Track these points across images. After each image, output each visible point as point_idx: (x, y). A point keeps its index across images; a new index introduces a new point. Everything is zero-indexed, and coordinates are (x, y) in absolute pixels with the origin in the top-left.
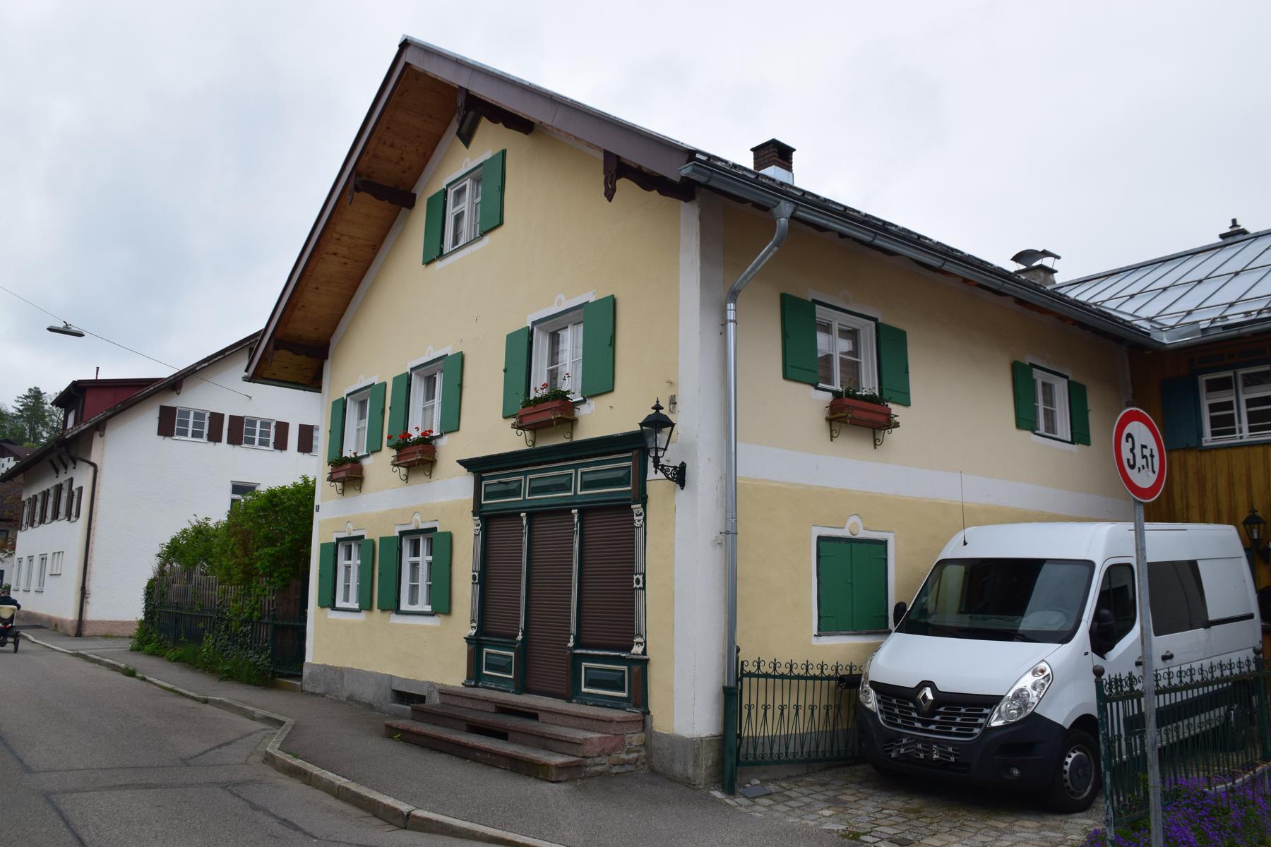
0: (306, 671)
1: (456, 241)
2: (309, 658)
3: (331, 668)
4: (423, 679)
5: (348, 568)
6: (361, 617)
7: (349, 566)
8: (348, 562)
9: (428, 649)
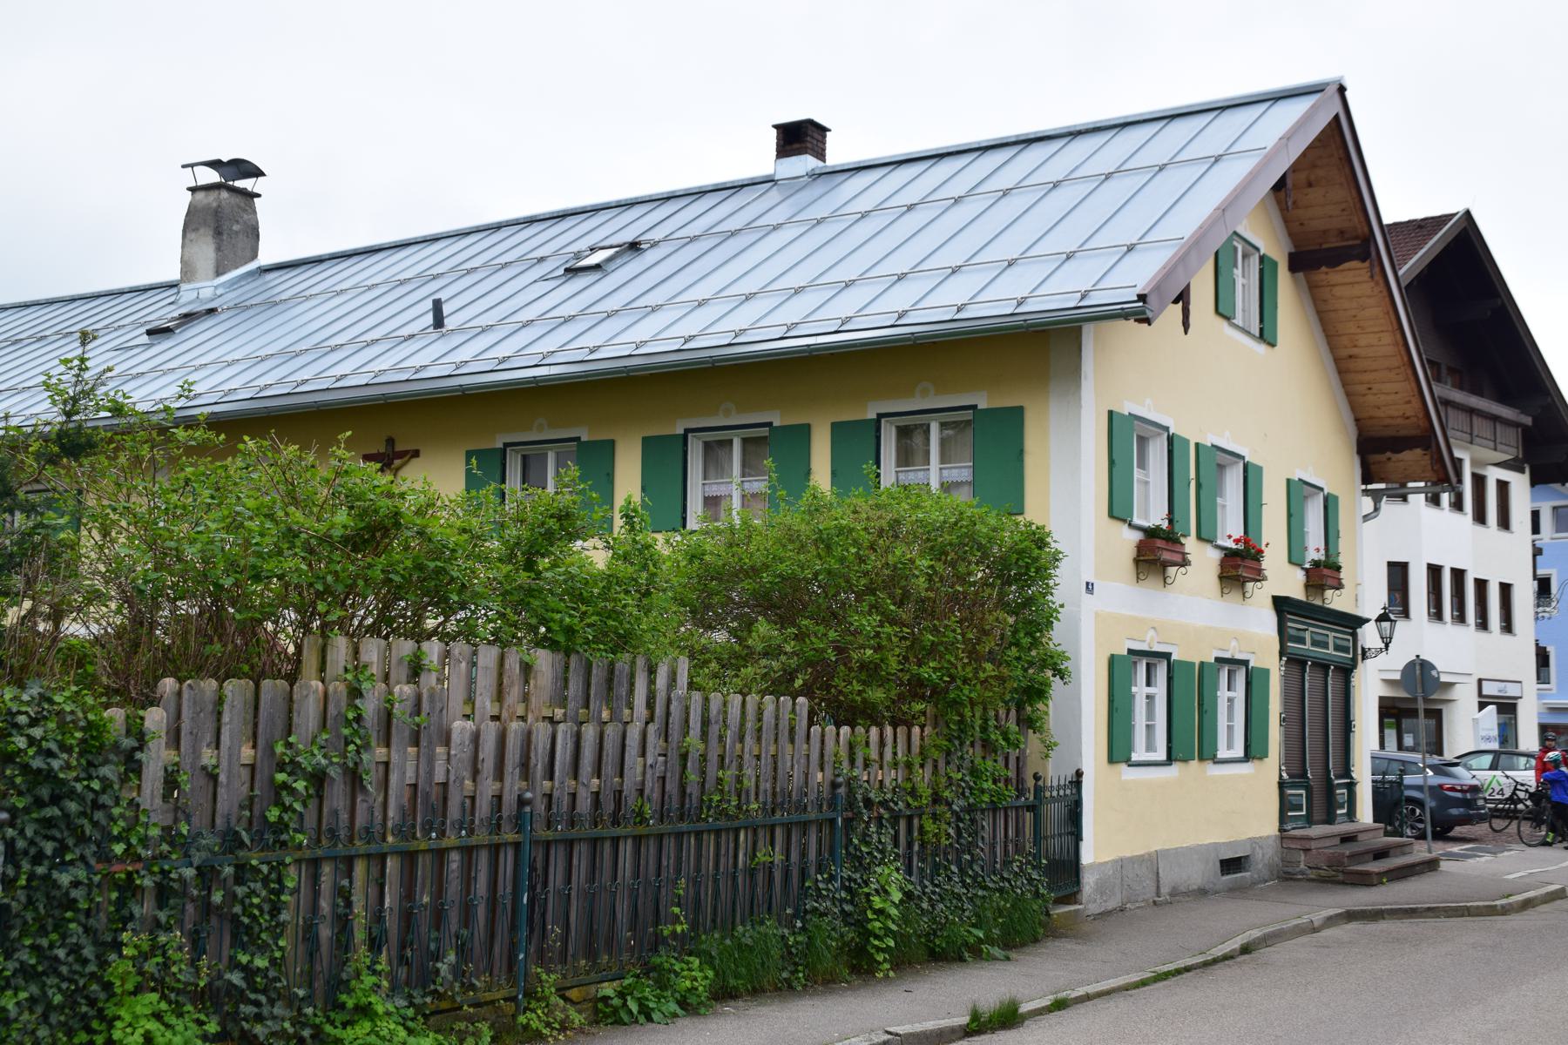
0: (1089, 881)
1: (1447, 403)
2: (1088, 856)
3: (1132, 860)
4: (1244, 837)
5: (1230, 700)
6: (1175, 770)
7: (1149, 697)
8: (1231, 694)
9: (1238, 802)
